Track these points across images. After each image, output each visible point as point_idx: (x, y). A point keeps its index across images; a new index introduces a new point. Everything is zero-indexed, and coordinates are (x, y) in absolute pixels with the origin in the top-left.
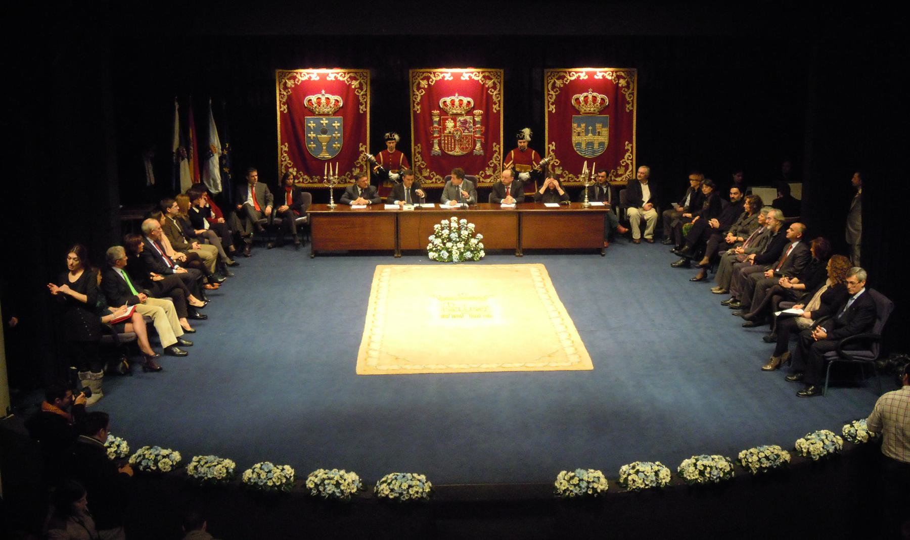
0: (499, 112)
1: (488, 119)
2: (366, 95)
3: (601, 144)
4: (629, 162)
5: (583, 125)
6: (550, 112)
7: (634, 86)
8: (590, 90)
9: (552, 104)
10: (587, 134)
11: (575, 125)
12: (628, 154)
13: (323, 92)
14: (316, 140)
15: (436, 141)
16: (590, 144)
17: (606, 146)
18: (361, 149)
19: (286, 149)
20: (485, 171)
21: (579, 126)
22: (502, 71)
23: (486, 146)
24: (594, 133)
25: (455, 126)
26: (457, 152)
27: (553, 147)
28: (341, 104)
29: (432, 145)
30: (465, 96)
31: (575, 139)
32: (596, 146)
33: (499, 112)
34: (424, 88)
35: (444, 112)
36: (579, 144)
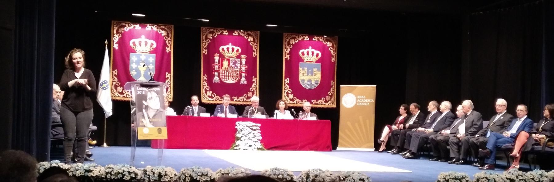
0: (170, 52)
1: (250, 62)
2: (171, 41)
3: (316, 81)
4: (255, 89)
5: (306, 69)
6: (286, 59)
7: (172, 35)
8: (310, 47)
9: (288, 54)
10: (308, 74)
11: (301, 69)
12: (168, 80)
13: (310, 47)
14: (137, 70)
15: (216, 73)
16: (310, 81)
17: (319, 83)
18: (167, 76)
19: (116, 74)
20: (247, 94)
21: (303, 69)
22: (173, 26)
23: (249, 79)
24: (312, 74)
25: (229, 64)
26: (230, 81)
27: (205, 78)
28: (155, 46)
29: (214, 76)
30: (316, 49)
31: (301, 77)
32: (313, 82)
33: (170, 52)
34: (210, 39)
35: (222, 57)
36: (303, 80)
